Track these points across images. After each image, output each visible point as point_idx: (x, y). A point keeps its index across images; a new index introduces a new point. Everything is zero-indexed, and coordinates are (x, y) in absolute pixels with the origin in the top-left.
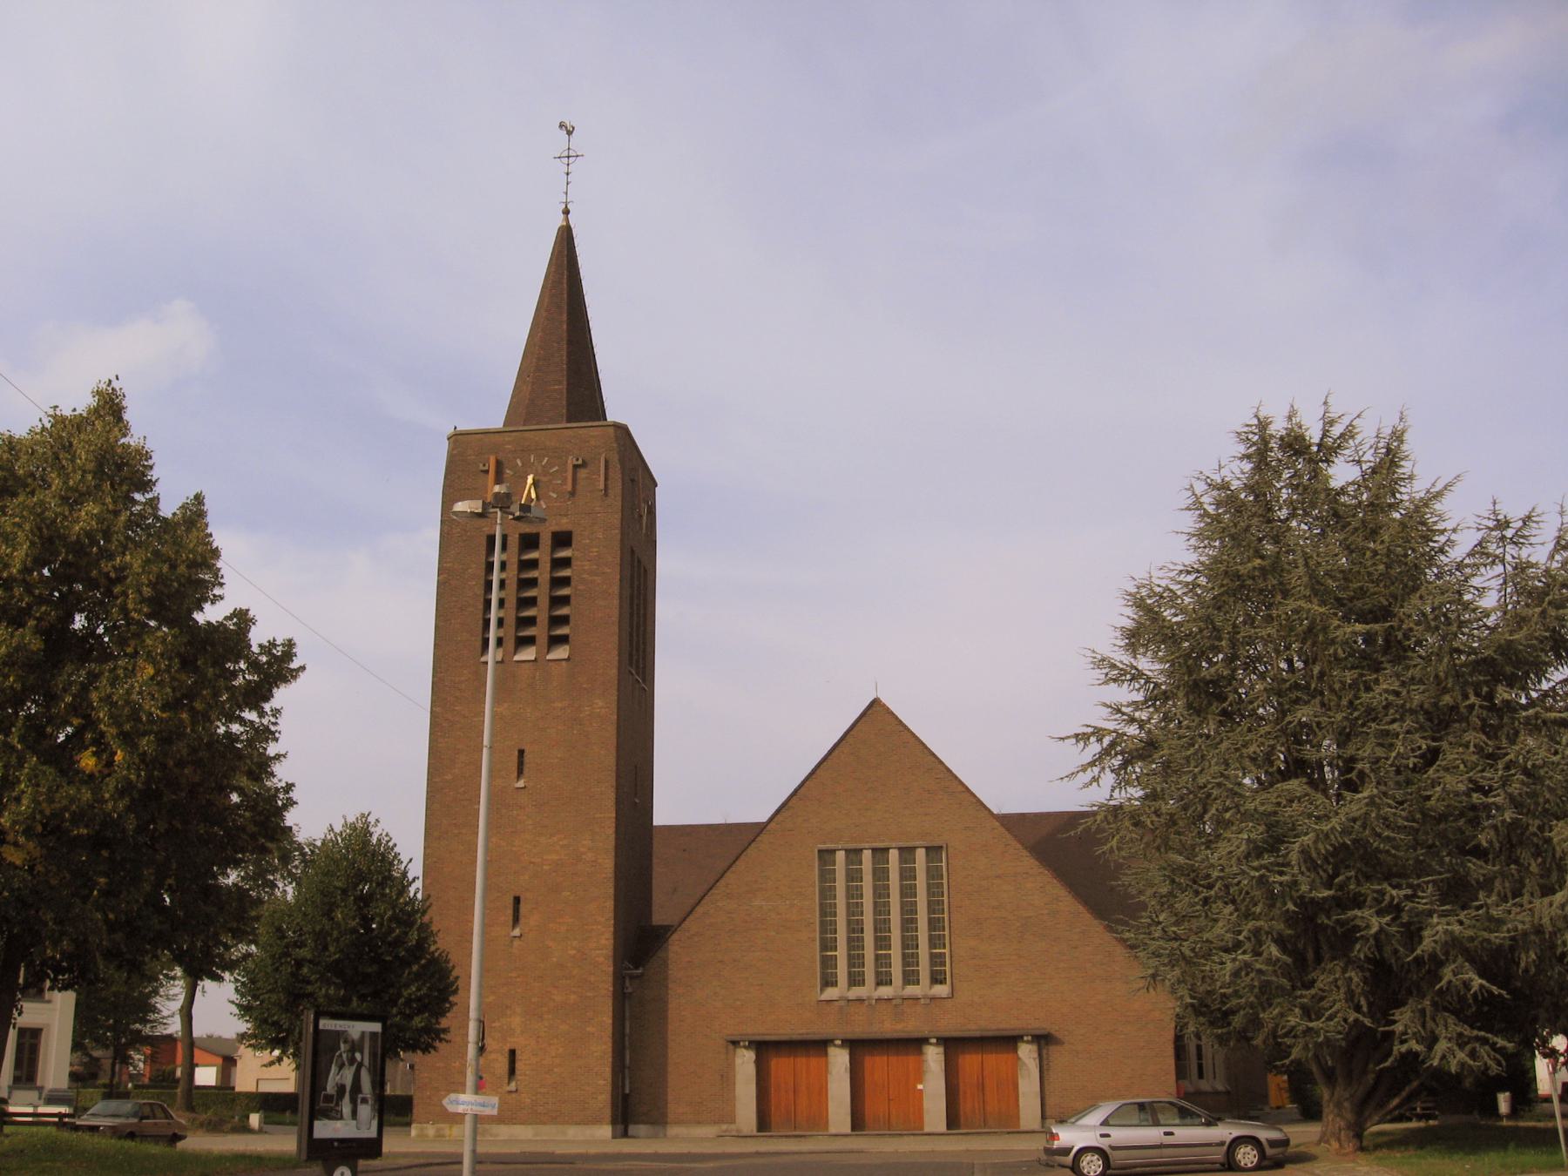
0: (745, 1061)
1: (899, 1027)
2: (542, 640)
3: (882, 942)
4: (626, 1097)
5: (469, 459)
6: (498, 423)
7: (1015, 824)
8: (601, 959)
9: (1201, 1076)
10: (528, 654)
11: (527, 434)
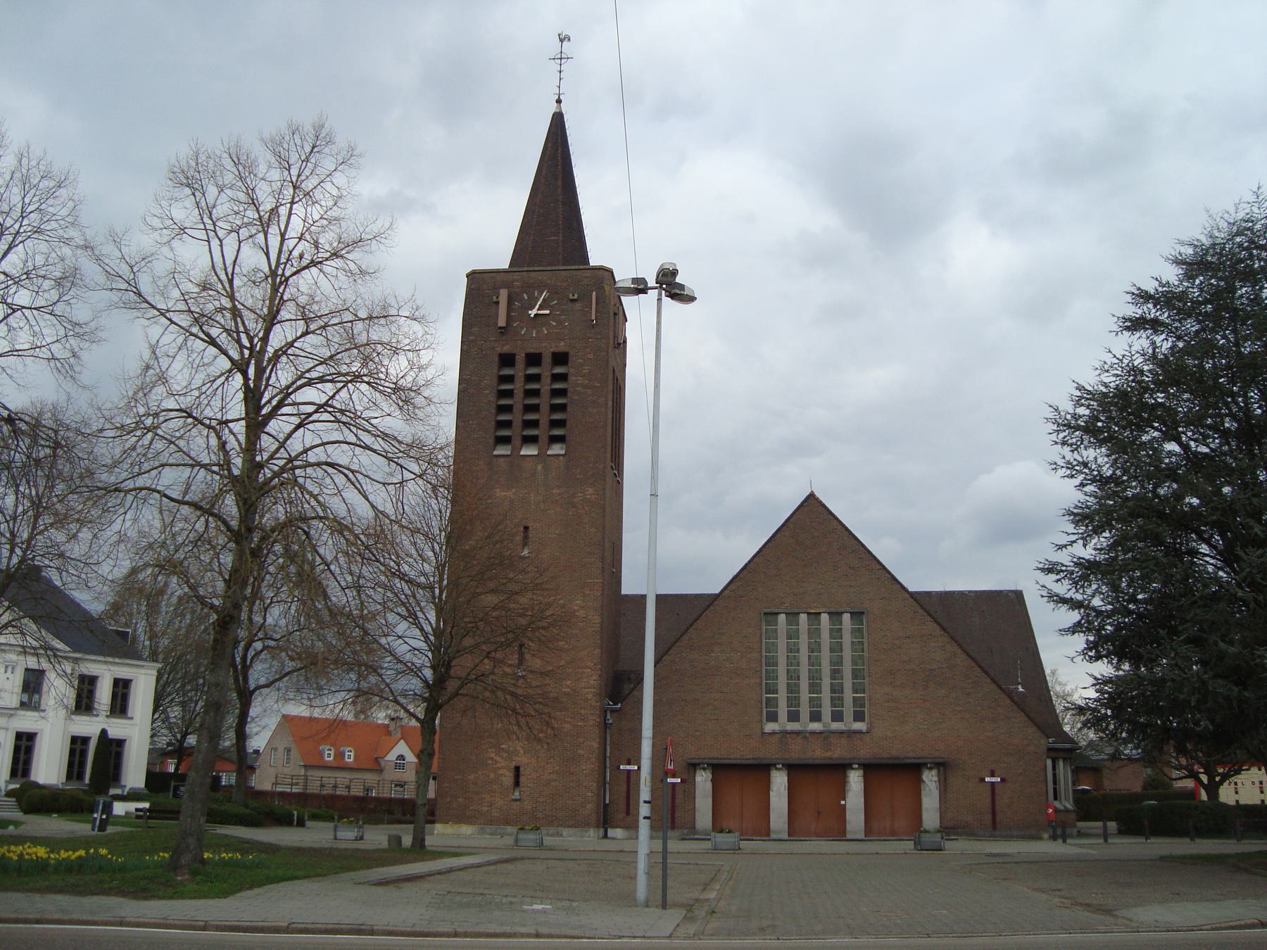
0: (703, 780)
1: (829, 754)
2: (544, 439)
3: (815, 687)
4: (606, 806)
5: (481, 286)
6: (506, 266)
7: (924, 601)
8: (590, 696)
9: (1055, 798)
10: (502, 450)
11: (532, 274)
